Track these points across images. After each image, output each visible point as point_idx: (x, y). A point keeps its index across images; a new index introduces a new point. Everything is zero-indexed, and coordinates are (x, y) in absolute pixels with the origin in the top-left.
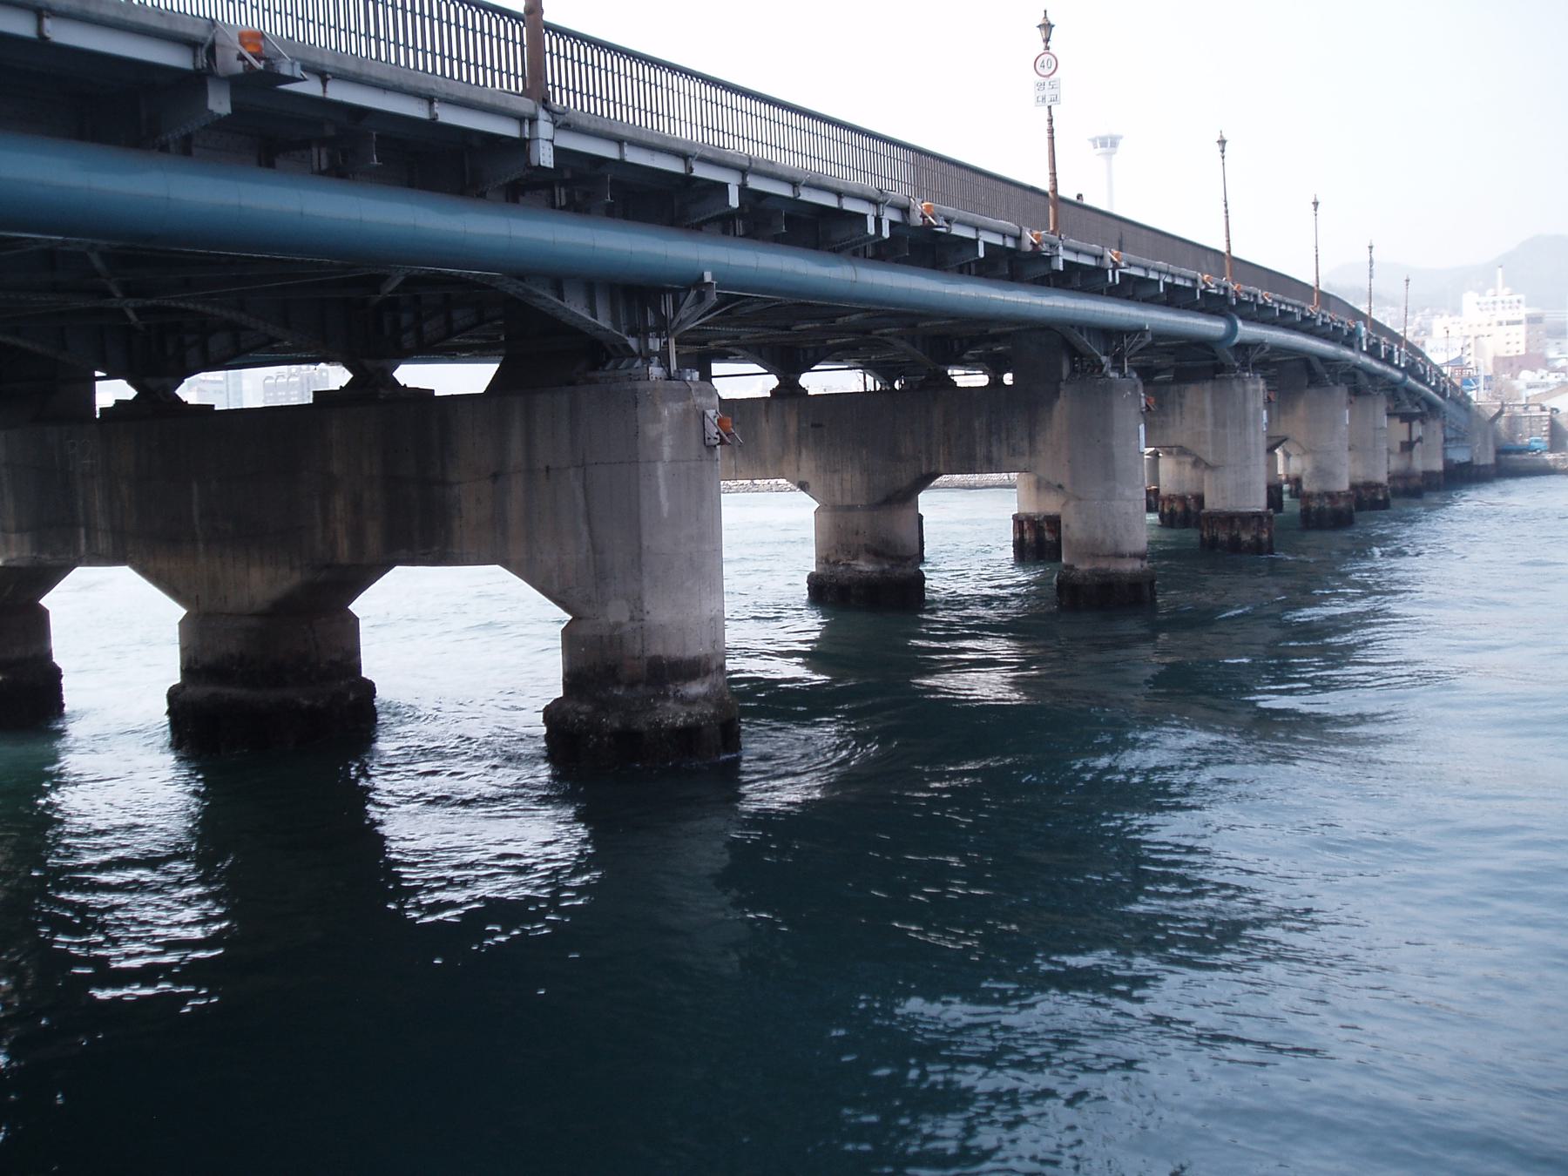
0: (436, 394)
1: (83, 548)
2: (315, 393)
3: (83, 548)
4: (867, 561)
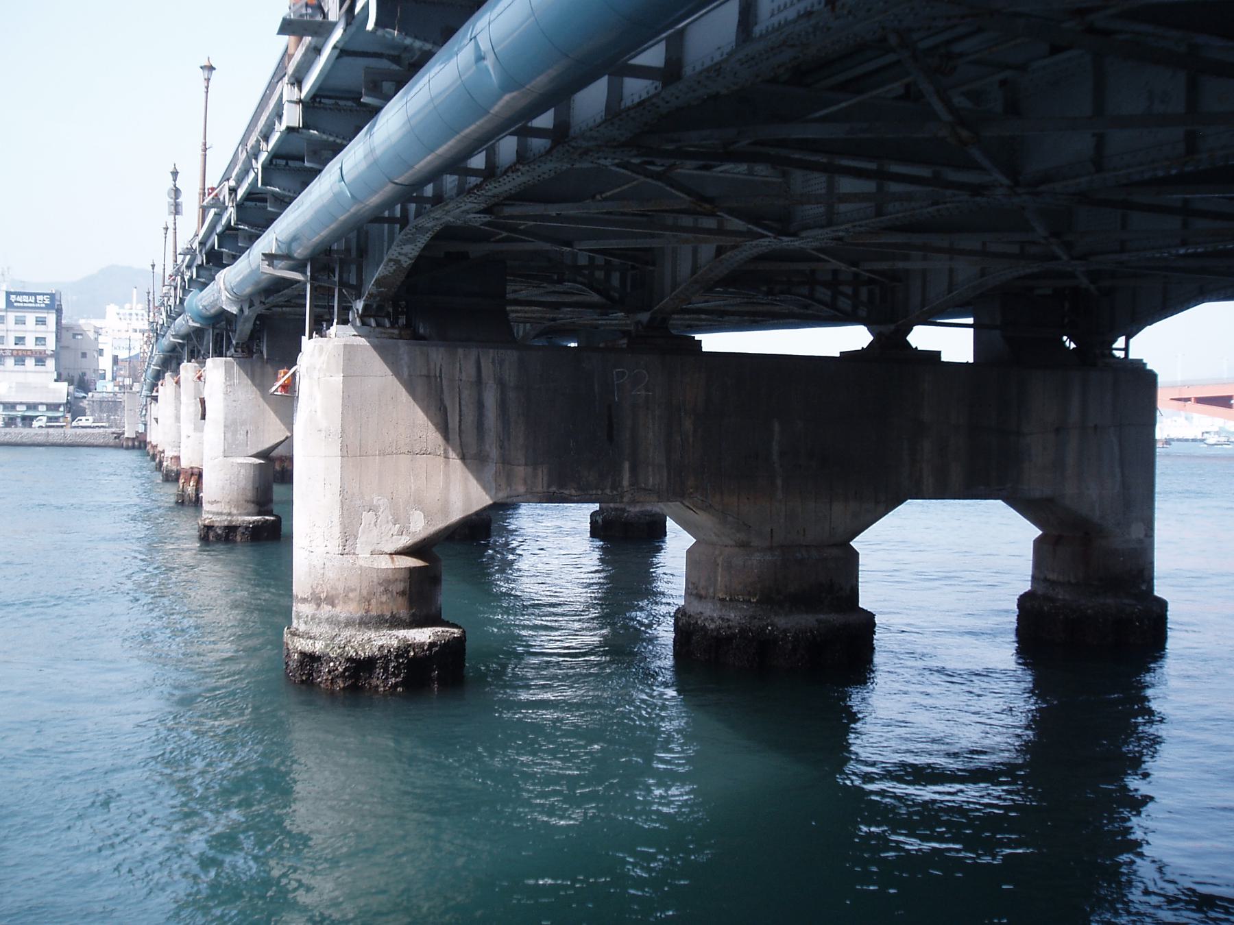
1: (626, 483)
2: (701, 341)
3: (626, 483)
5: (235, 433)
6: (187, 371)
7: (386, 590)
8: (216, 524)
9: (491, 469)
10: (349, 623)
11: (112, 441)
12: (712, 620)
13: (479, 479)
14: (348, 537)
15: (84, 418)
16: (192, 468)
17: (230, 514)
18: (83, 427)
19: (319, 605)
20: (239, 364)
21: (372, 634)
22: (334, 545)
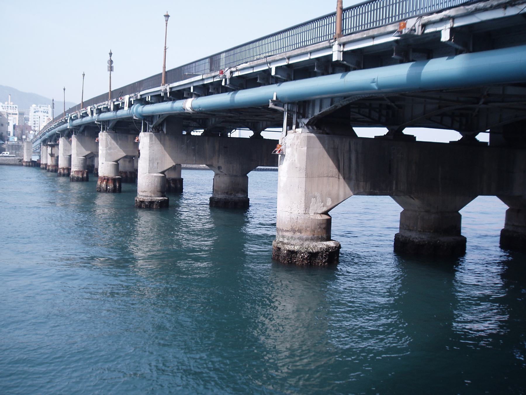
0: (417, 140)
1: (394, 188)
3: (394, 188)
4: (241, 194)
5: (153, 163)
6: (102, 136)
7: (320, 227)
8: (146, 201)
9: (353, 182)
10: (307, 239)
11: (18, 163)
12: (416, 238)
13: (349, 186)
14: (307, 208)
15: (5, 153)
16: (104, 176)
17: (151, 196)
18: (5, 156)
19: (294, 233)
20: (155, 135)
21: (315, 243)
22: (302, 211)
